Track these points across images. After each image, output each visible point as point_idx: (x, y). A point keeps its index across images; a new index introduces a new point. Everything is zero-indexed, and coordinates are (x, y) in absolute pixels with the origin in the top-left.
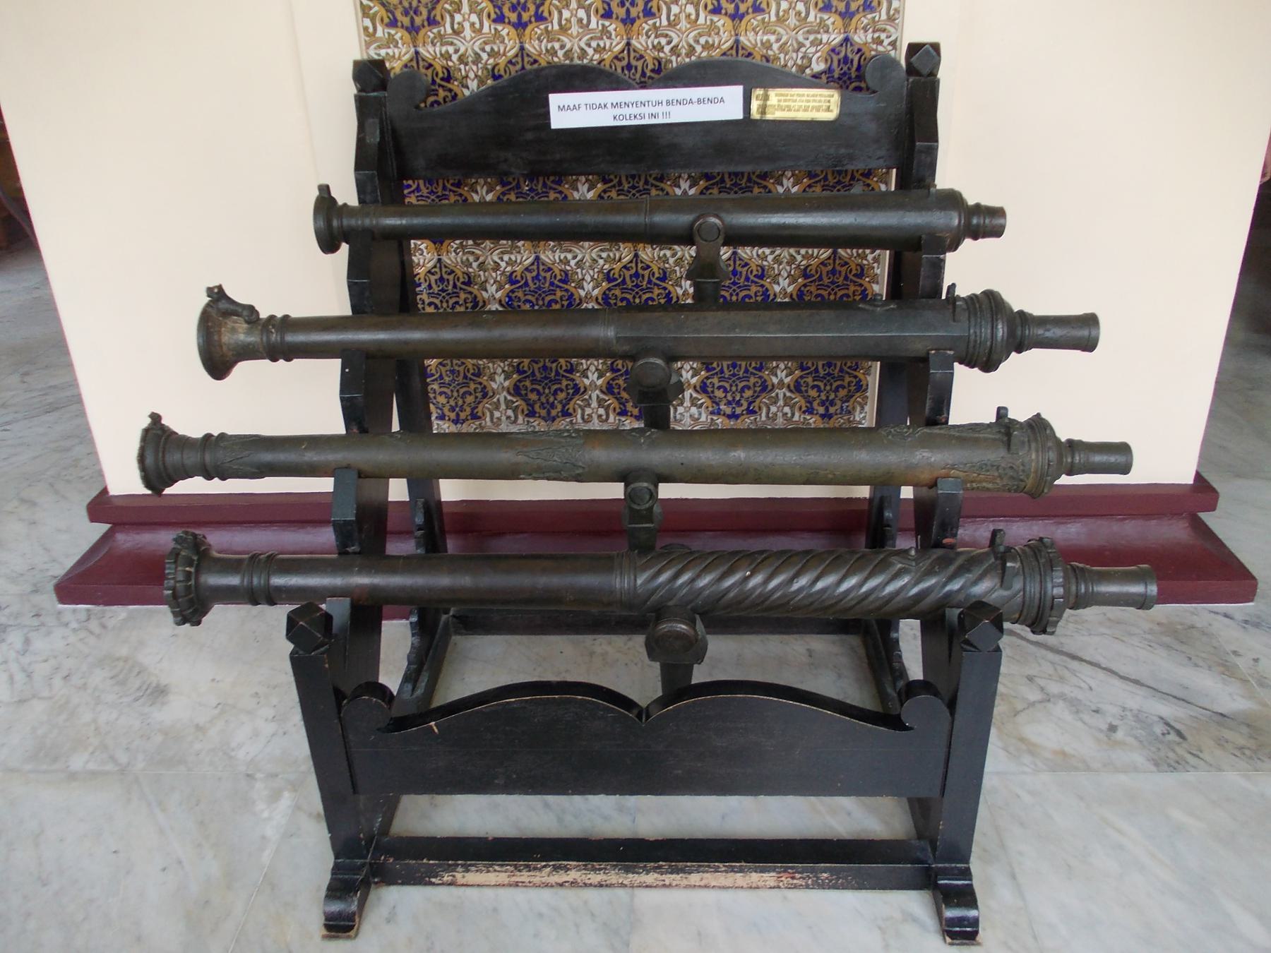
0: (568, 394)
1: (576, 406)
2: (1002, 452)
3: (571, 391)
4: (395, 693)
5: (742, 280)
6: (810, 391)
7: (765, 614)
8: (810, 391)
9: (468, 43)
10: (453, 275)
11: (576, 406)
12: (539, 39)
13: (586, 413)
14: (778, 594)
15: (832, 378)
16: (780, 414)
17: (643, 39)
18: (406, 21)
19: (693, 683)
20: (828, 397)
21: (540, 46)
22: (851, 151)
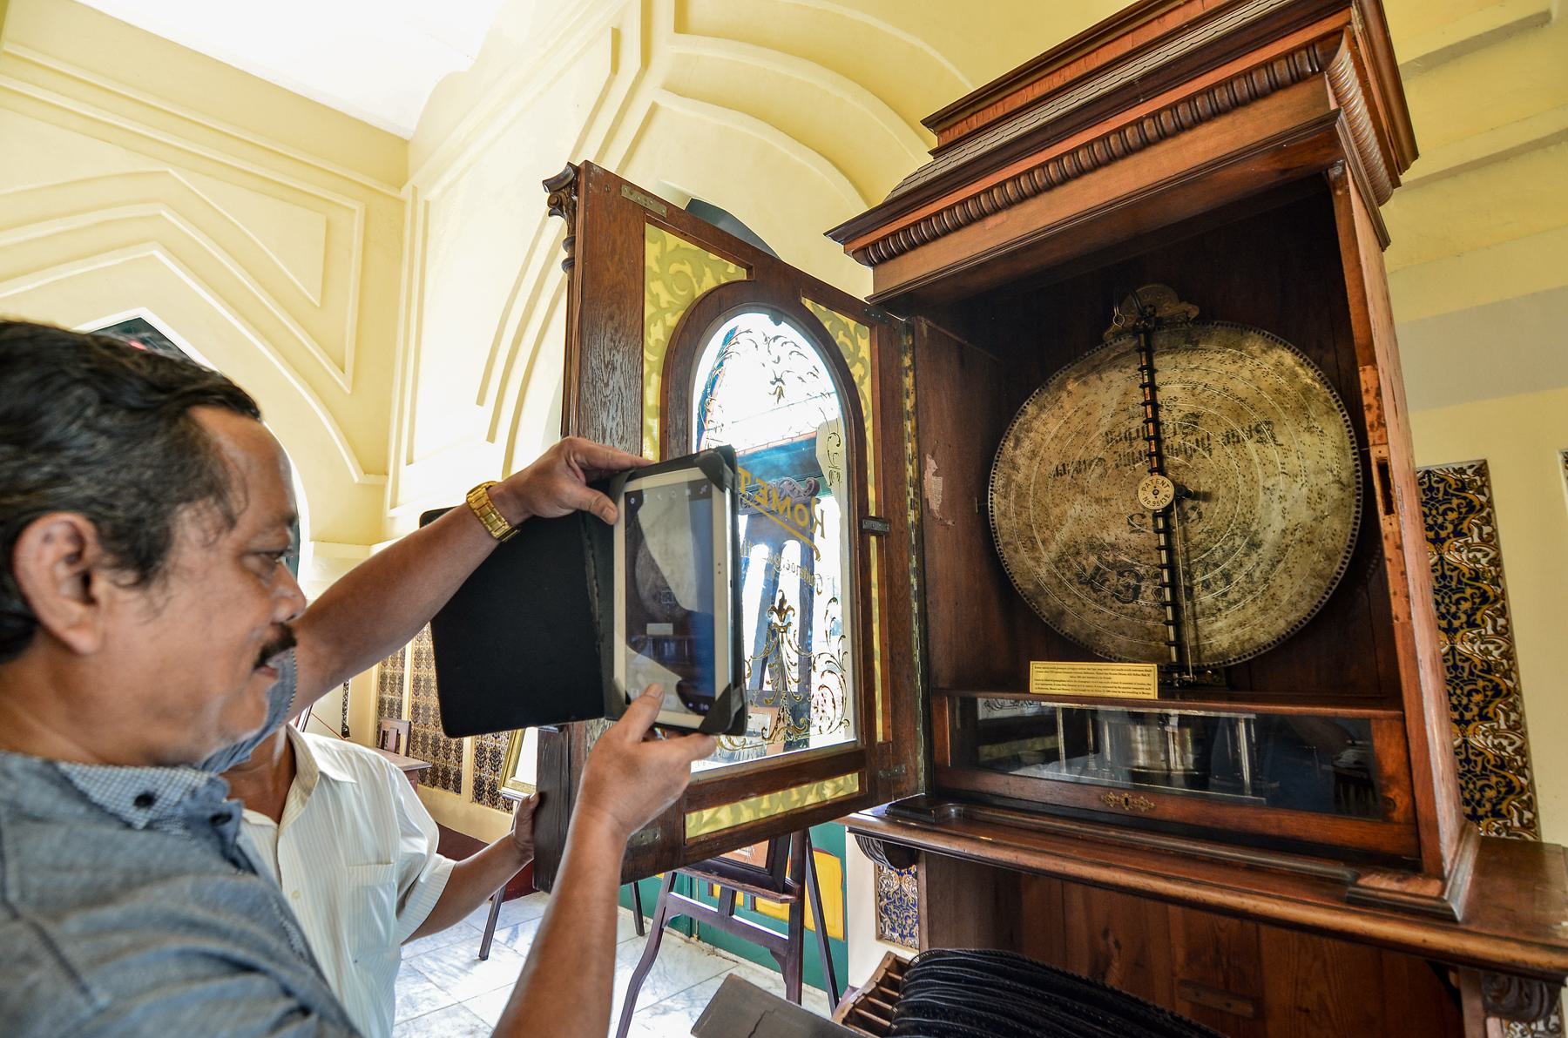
0: (1486, 696)
1: (1511, 807)
3: (1503, 790)
4: (427, 628)
10: (1457, 572)
11: (1511, 807)
13: (1525, 817)
14: (147, 420)
15: (1437, 502)
19: (766, 844)
20: (1448, 611)
22: (1297, 368)
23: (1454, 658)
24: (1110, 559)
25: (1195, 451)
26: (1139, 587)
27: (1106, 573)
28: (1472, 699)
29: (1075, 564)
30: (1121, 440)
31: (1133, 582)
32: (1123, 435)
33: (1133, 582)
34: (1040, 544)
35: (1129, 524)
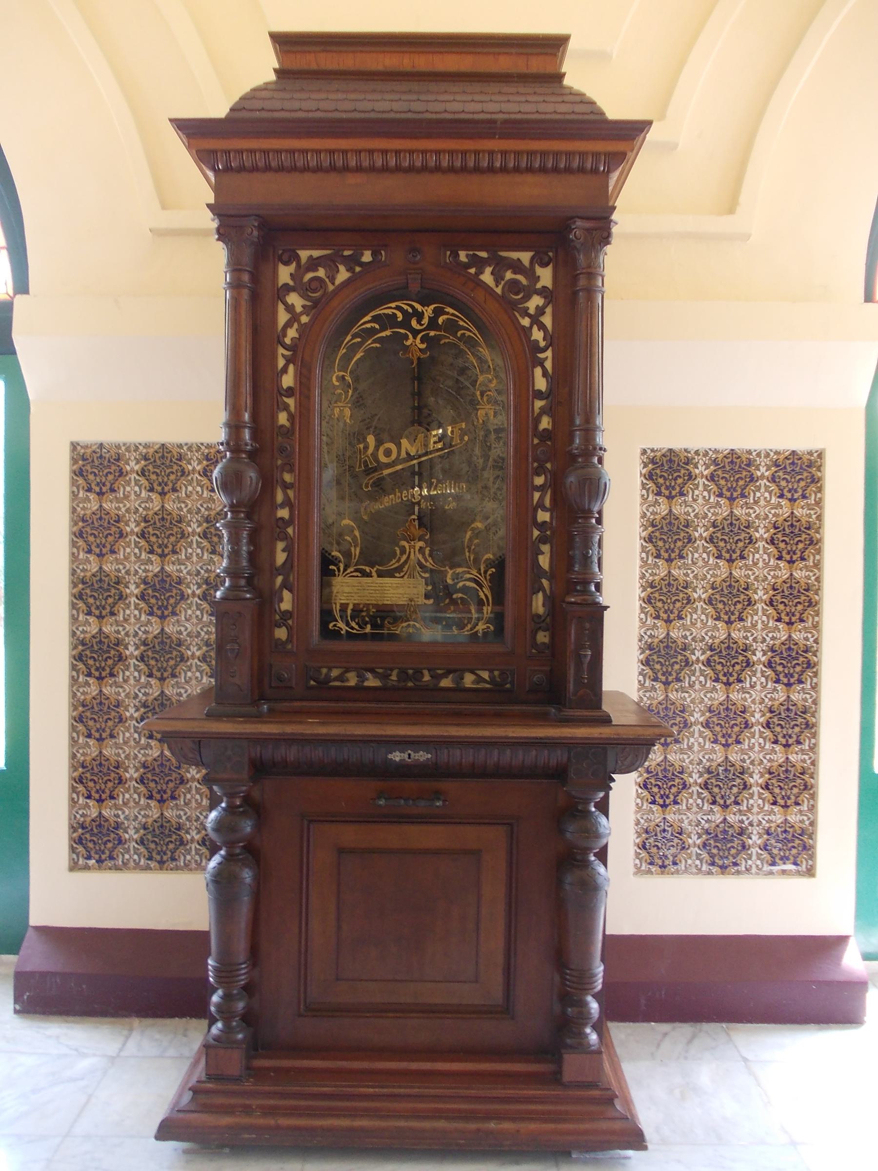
2: (527, 689)
5: (735, 591)
6: (718, 604)
7: (364, 327)
8: (718, 604)
9: (699, 507)
12: (737, 691)
16: (760, 621)
17: (793, 816)
18: (722, 802)
20: (163, 542)
21: (681, 510)
23: (162, 820)
24: (481, 461)
25: (376, 428)
26: (495, 430)
27: (495, 461)
28: (671, 791)
29: (496, 486)
30: (381, 488)
31: (493, 436)
32: (376, 489)
33: (493, 436)
34: (489, 521)
35: (448, 457)
